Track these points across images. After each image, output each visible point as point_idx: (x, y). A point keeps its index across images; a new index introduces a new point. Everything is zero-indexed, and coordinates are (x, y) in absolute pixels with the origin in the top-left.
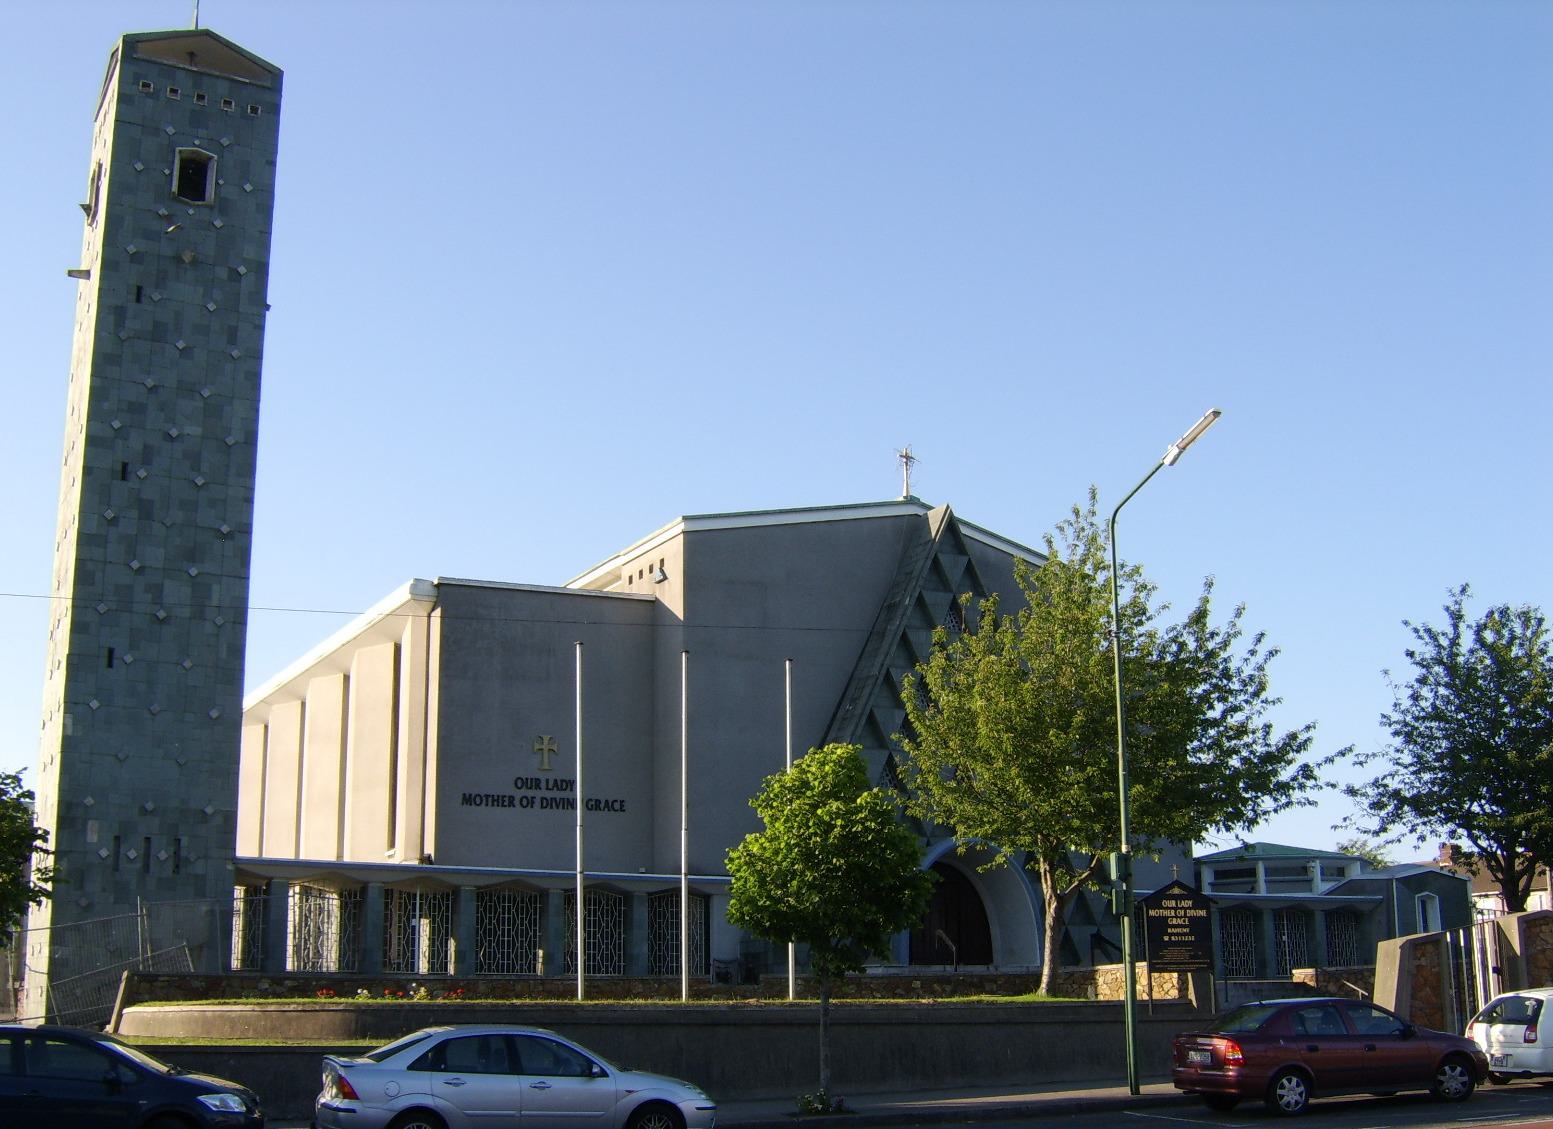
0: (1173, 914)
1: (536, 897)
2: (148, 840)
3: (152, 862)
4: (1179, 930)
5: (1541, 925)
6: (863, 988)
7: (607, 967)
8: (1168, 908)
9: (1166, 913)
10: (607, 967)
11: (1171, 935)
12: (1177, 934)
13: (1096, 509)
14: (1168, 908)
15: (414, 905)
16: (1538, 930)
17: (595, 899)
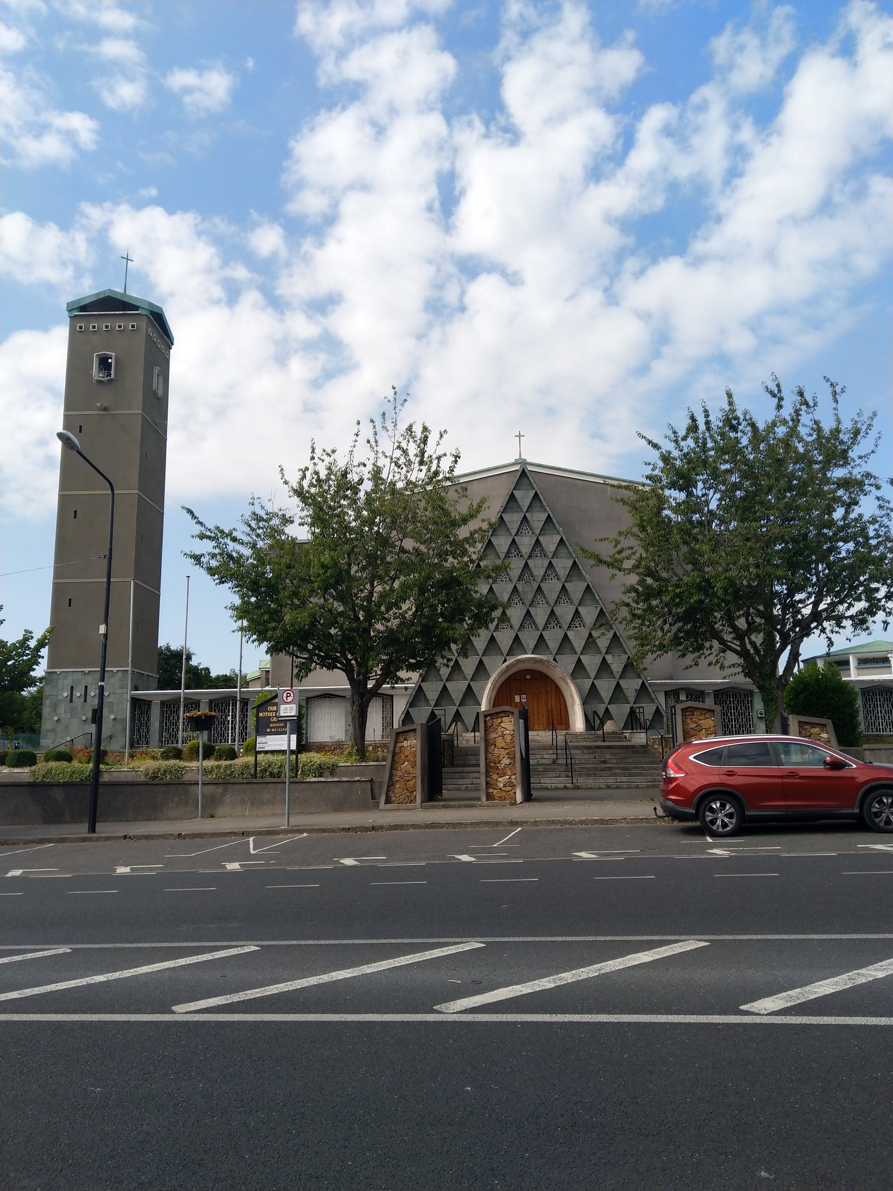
0: (274, 715)
1: (747, 694)
2: (86, 687)
3: (88, 697)
4: (277, 725)
5: (502, 717)
6: (831, 756)
7: (173, 741)
8: (271, 711)
9: (270, 714)
10: (173, 741)
11: (271, 728)
12: (276, 727)
13: (393, 390)
14: (271, 711)
15: (229, 709)
16: (500, 720)
17: (879, 692)
